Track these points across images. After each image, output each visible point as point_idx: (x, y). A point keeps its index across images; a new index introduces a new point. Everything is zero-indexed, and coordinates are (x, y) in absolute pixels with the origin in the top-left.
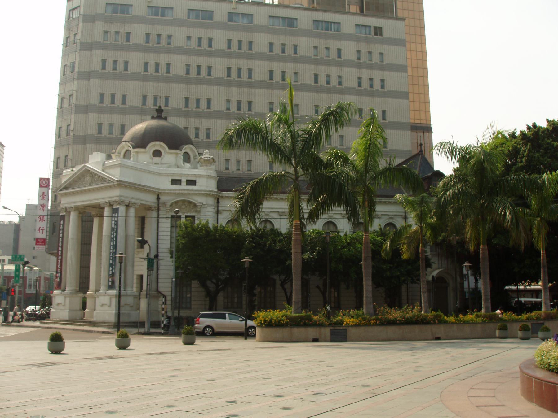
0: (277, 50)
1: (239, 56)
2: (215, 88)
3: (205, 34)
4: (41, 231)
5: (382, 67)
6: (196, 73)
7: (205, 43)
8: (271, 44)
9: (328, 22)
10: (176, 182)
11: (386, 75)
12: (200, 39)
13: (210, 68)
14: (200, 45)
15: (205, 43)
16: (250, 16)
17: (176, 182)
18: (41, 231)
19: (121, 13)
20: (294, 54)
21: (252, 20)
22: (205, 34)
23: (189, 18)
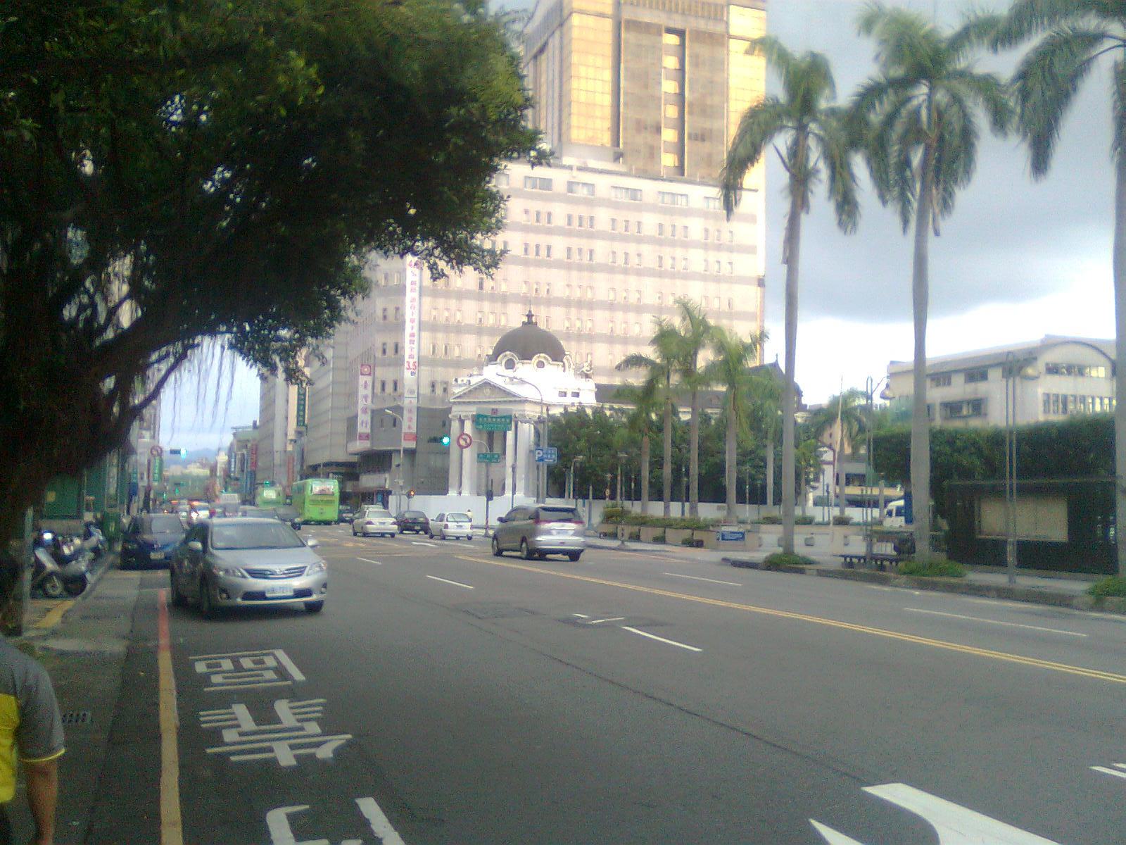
0: (620, 228)
1: (579, 235)
2: (554, 271)
3: (543, 207)
4: (364, 425)
5: (731, 249)
6: (535, 254)
7: (544, 218)
8: (661, 226)
9: (635, 190)
10: (564, 394)
11: (735, 257)
12: (538, 213)
13: (549, 248)
14: (538, 221)
15: (544, 218)
16: (591, 186)
17: (564, 394)
18: (364, 425)
19: (540, 189)
20: (626, 231)
21: (593, 191)
22: (543, 207)
23: (525, 186)
